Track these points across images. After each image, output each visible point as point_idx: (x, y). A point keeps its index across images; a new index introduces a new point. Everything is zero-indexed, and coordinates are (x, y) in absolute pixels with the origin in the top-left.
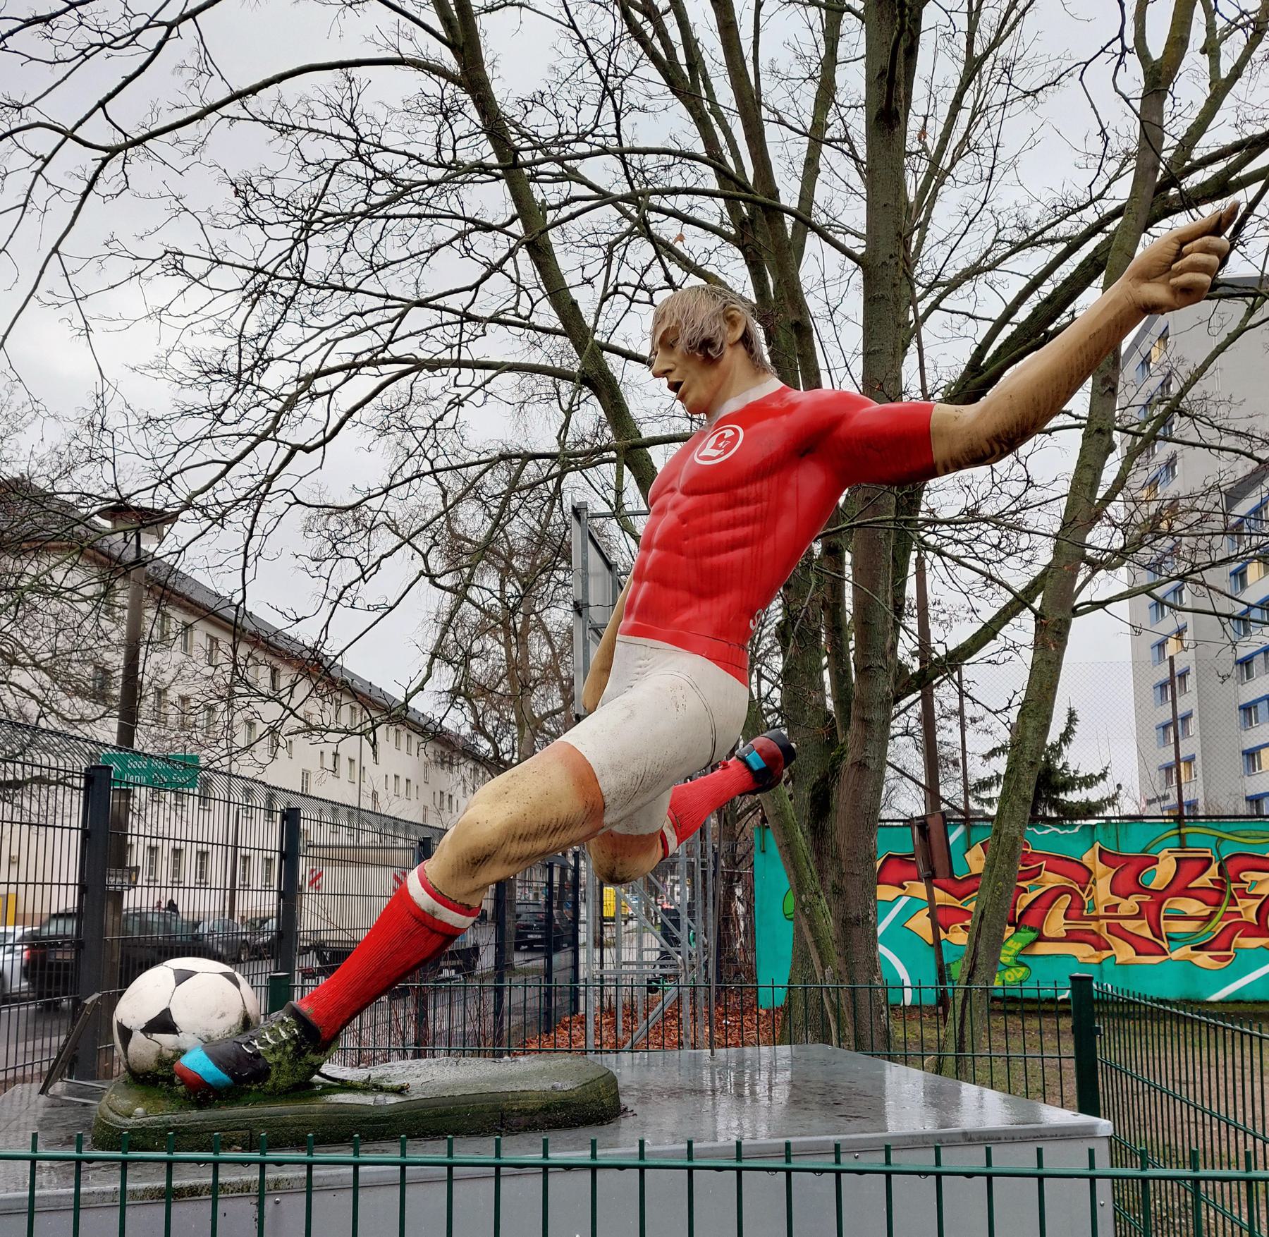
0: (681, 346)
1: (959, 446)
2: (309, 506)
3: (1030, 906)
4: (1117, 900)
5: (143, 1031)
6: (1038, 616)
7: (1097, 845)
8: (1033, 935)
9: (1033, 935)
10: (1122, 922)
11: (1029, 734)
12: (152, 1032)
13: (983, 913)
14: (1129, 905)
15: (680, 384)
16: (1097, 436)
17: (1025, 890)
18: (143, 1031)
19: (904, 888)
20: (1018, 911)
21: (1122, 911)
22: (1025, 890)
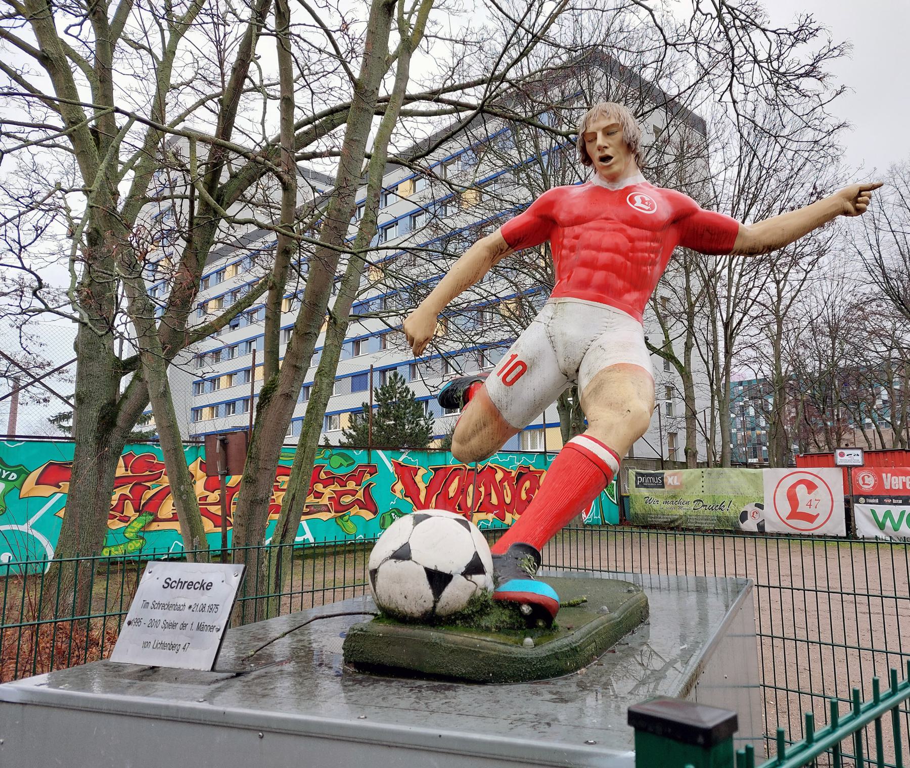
0: (618, 136)
1: (748, 244)
2: (263, 123)
3: (150, 499)
4: (207, 493)
5: (464, 574)
6: (129, 313)
7: (200, 459)
8: (151, 518)
9: (151, 518)
10: (208, 507)
11: (324, 387)
12: (471, 574)
13: (294, 495)
14: (214, 496)
15: (611, 158)
16: (370, 224)
17: (149, 488)
18: (464, 574)
19: (59, 487)
20: (143, 502)
21: (209, 500)
22: (149, 488)
